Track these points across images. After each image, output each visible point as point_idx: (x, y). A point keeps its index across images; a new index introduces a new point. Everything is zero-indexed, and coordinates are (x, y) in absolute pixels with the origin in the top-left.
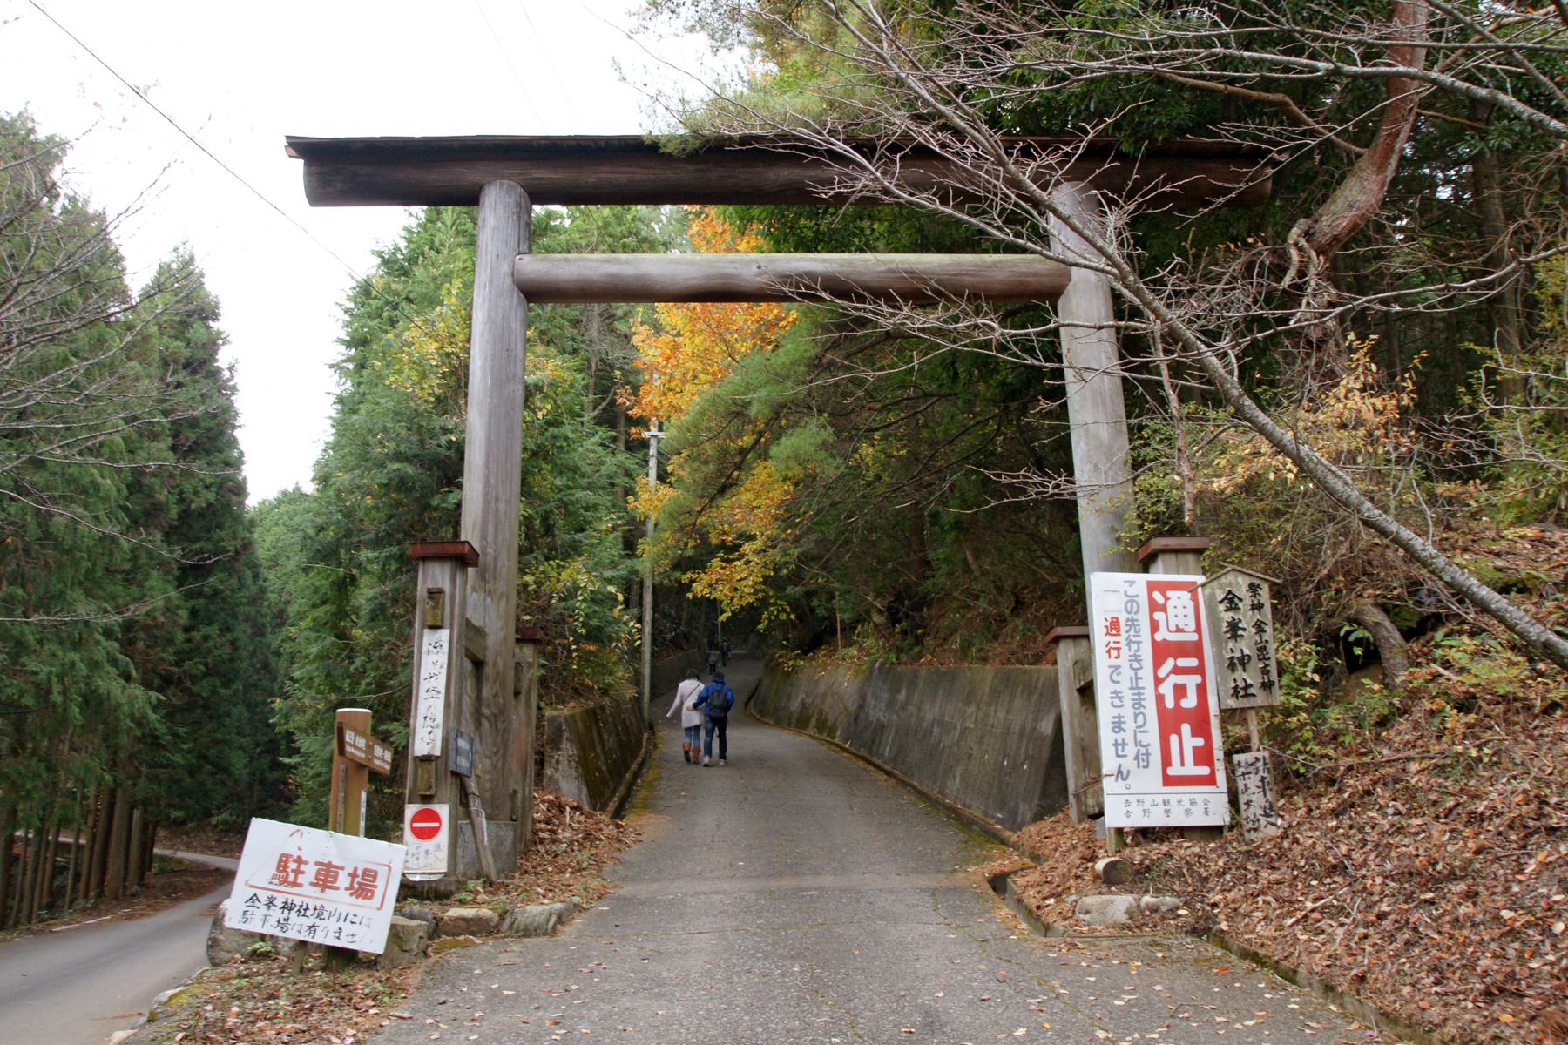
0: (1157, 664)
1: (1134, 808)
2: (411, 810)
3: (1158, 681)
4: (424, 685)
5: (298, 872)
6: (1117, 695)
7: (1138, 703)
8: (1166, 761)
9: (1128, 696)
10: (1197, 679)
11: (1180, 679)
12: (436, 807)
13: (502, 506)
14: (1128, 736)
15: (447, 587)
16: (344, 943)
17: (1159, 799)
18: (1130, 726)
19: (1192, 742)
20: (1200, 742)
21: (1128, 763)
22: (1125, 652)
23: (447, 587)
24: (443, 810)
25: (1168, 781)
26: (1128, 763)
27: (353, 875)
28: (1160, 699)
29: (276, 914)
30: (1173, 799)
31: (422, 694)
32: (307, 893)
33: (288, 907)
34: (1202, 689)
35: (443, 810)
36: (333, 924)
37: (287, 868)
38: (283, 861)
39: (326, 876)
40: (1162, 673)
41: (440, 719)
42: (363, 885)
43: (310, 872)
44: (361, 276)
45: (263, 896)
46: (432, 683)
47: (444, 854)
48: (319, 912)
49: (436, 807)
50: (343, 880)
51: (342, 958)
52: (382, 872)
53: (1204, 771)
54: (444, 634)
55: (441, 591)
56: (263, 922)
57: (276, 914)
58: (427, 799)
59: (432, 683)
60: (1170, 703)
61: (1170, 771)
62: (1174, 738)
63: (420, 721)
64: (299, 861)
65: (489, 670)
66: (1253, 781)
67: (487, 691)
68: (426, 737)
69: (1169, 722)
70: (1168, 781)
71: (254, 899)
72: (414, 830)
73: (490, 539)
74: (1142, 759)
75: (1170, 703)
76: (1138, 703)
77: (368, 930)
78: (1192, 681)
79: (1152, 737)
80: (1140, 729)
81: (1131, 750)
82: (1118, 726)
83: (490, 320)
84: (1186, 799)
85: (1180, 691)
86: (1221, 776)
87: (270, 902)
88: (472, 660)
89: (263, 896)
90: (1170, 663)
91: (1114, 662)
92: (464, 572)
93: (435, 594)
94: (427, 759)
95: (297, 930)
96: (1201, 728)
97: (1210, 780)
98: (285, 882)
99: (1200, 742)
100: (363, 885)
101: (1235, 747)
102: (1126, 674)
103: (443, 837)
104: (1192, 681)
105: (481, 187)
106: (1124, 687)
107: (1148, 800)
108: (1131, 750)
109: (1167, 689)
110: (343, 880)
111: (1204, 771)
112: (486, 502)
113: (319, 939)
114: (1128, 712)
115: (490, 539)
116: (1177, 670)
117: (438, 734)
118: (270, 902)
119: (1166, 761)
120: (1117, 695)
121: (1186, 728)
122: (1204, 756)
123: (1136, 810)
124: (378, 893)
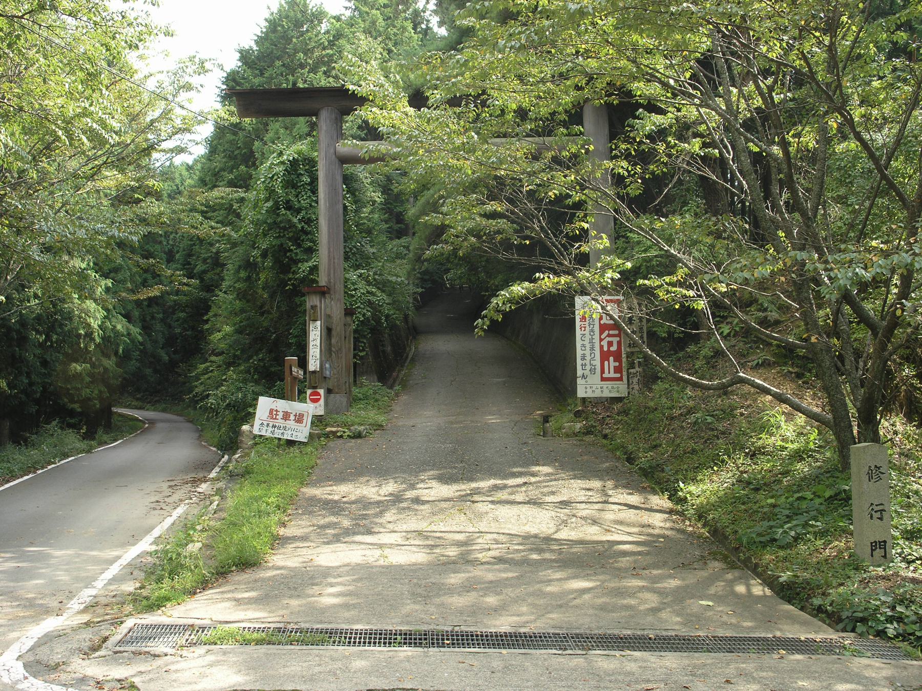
0: (601, 333)
1: (589, 390)
2: (309, 392)
3: (601, 340)
4: (311, 344)
5: (276, 415)
6: (583, 345)
7: (592, 349)
8: (603, 372)
9: (588, 346)
10: (618, 339)
11: (610, 339)
12: (319, 390)
13: (336, 261)
14: (588, 362)
15: (318, 304)
16: (293, 438)
17: (599, 386)
18: (588, 358)
19: (613, 364)
20: (617, 364)
21: (587, 372)
22: (588, 329)
23: (318, 304)
24: (322, 392)
25: (603, 379)
26: (587, 372)
27: (295, 416)
28: (601, 347)
29: (270, 429)
30: (605, 387)
31: (311, 347)
32: (280, 422)
33: (274, 426)
34: (619, 343)
35: (322, 392)
36: (290, 432)
37: (272, 413)
38: (271, 411)
39: (286, 416)
40: (603, 337)
41: (318, 357)
42: (299, 419)
43: (281, 415)
44: (228, 69)
45: (265, 423)
46: (315, 343)
47: (323, 408)
48: (285, 428)
49: (319, 390)
50: (292, 417)
51: (291, 443)
52: (306, 414)
53: (618, 375)
54: (318, 323)
55: (316, 306)
56: (267, 432)
57: (270, 429)
58: (315, 388)
59: (315, 343)
60: (605, 349)
61: (604, 376)
62: (606, 363)
63: (311, 357)
64: (277, 411)
65: (334, 333)
66: (635, 380)
67: (333, 341)
68: (314, 364)
69: (605, 356)
70: (603, 379)
71: (262, 424)
72: (311, 400)
73: (332, 276)
74: (593, 371)
75: (605, 349)
76: (592, 349)
77: (301, 433)
78: (615, 340)
79: (597, 363)
80: (593, 359)
81: (588, 367)
82: (583, 358)
83: (326, 176)
84: (610, 387)
85: (610, 344)
86: (625, 378)
87: (268, 425)
88: (328, 332)
89: (265, 423)
90: (607, 332)
91: (583, 332)
92: (325, 298)
93: (314, 307)
94: (314, 372)
95: (278, 434)
96: (618, 358)
97: (620, 379)
98: (272, 418)
99: (617, 364)
100: (299, 419)
101: (631, 365)
102: (588, 337)
103: (322, 402)
104: (615, 340)
105: (319, 110)
106: (587, 343)
107: (594, 387)
108: (588, 367)
109: (604, 343)
110: (292, 417)
111: (618, 375)
112: (329, 260)
113: (285, 437)
114: (588, 352)
115: (332, 276)
116: (609, 336)
117: (318, 362)
118: (268, 425)
119: (603, 372)
120: (583, 345)
121: (611, 359)
122: (618, 370)
123: (589, 390)
124: (305, 421)
